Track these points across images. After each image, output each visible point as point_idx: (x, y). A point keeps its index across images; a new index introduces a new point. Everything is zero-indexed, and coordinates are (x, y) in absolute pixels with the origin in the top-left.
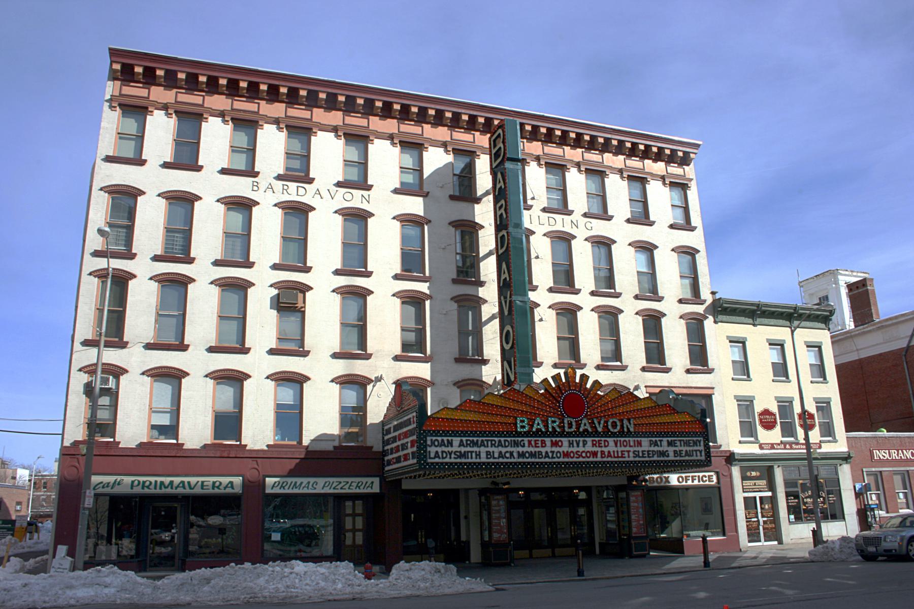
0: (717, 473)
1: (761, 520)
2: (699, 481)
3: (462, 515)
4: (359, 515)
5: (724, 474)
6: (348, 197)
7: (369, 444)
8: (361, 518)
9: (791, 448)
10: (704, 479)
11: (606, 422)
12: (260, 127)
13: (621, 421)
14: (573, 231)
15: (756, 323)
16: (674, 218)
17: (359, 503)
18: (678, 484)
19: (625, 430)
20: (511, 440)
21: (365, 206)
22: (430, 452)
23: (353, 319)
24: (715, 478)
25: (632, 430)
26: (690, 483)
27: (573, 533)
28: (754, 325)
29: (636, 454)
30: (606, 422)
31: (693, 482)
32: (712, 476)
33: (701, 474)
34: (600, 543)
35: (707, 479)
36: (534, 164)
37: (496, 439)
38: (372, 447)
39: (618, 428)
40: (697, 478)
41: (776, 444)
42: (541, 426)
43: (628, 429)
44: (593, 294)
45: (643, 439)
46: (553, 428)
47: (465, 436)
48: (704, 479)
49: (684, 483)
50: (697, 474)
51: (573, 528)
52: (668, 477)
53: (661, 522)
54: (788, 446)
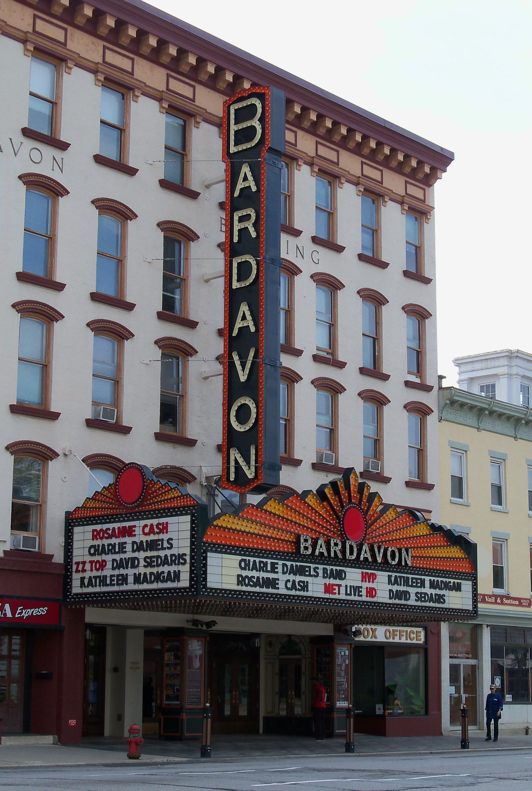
0: (426, 629)
1: (464, 696)
2: (406, 639)
3: (109, 664)
4: (16, 657)
5: (433, 631)
6: (36, 156)
7: (48, 552)
8: (17, 662)
9: (502, 603)
10: (412, 636)
11: (386, 550)
12: (67, 70)
13: (400, 550)
14: (298, 262)
15: (482, 426)
16: (363, 247)
17: (16, 640)
18: (385, 640)
19: (403, 564)
20: (121, 559)
21: (56, 176)
22: (458, 588)
23: (108, 370)
24: (423, 634)
25: (409, 563)
26: (397, 640)
27: (234, 702)
28: (515, 438)
29: (420, 597)
30: (386, 550)
31: (400, 639)
32: (420, 632)
33: (409, 629)
34: (264, 718)
35: (415, 635)
36: (305, 169)
37: (252, 559)
38: (52, 556)
39: (397, 560)
40: (405, 633)
41: (487, 595)
42: (324, 550)
43: (406, 561)
44: (362, 371)
45: (463, 582)
46: (335, 552)
47: (258, 557)
48: (412, 636)
49: (391, 640)
50: (405, 629)
51: (234, 693)
52: (376, 629)
53: (211, 700)
54: (499, 601)
